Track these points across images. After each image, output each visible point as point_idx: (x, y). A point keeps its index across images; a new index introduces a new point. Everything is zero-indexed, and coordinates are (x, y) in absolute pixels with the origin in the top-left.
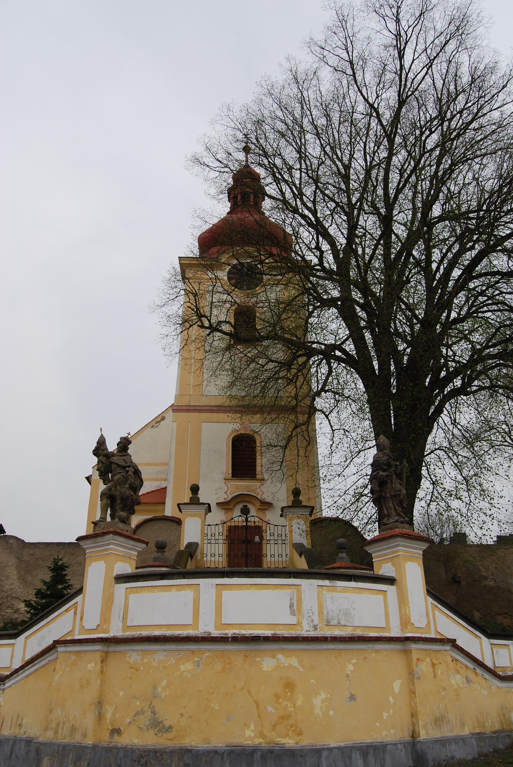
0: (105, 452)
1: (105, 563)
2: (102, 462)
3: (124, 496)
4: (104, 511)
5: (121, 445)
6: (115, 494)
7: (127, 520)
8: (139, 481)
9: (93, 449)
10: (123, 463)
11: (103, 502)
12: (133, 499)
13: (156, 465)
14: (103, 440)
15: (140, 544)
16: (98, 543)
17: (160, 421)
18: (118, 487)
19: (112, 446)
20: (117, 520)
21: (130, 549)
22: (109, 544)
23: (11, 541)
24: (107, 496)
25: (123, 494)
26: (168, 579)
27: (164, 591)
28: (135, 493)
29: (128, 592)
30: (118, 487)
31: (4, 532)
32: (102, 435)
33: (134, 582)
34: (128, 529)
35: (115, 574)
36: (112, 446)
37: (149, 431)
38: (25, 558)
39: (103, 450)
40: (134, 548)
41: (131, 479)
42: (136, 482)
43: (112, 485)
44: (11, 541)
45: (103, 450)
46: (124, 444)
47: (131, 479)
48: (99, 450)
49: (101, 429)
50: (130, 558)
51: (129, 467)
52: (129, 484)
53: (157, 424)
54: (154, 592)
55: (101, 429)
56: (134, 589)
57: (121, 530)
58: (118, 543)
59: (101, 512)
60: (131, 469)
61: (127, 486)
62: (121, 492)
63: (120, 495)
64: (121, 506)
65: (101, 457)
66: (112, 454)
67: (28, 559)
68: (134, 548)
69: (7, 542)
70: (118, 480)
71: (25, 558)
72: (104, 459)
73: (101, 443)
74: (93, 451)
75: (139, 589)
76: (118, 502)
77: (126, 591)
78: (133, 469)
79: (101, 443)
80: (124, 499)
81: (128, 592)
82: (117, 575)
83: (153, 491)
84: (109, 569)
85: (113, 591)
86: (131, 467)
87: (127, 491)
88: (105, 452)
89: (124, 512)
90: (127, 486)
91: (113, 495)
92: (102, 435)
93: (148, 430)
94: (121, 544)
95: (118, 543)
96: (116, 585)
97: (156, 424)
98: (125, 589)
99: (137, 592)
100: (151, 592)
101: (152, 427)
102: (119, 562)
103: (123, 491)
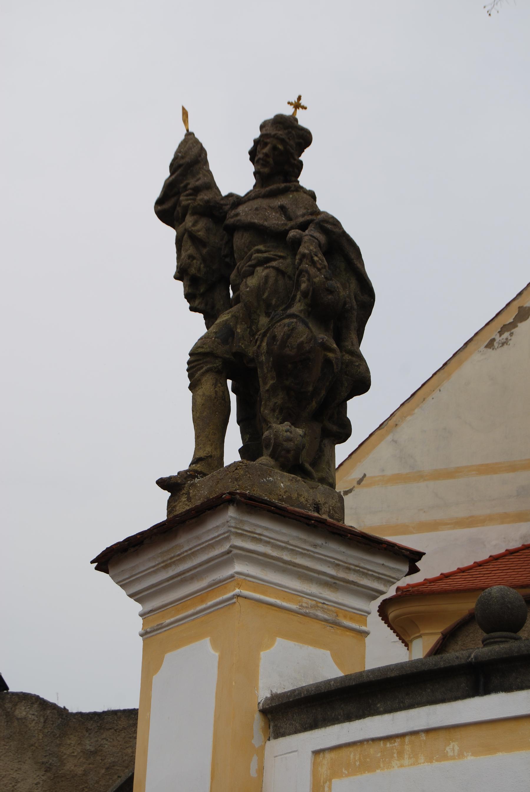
0: (204, 196)
1: (215, 644)
2: (194, 238)
3: (287, 351)
4: (209, 424)
5: (266, 150)
6: (251, 351)
7: (315, 463)
8: (353, 285)
9: (157, 192)
10: (275, 221)
11: (200, 392)
12: (328, 362)
13: (513, 468)
14: (195, 151)
15: (380, 560)
16: (183, 559)
17: (513, 325)
18: (264, 321)
19: (233, 175)
20: (265, 459)
21: (334, 584)
22: (228, 558)
23: (21, 711)
24: (218, 363)
25: (284, 343)
26: (508, 689)
27: (490, 749)
28: (339, 338)
29: (324, 770)
30: (264, 321)
31: (7, 688)
32: (189, 135)
33: (349, 718)
34: (320, 499)
35: (263, 693)
36: (233, 175)
37: (479, 361)
38: (69, 766)
39: (197, 190)
40: (352, 577)
41: (312, 271)
42: (335, 283)
43: (235, 317)
44: (21, 711)
45: (197, 190)
46: (281, 146)
47: (312, 271)
48: (178, 194)
49: (185, 114)
50: (336, 624)
51: (303, 227)
52: (305, 295)
53: (506, 335)
54: (445, 757)
55: (185, 114)
56: (353, 754)
57: (282, 500)
58: (268, 550)
59: (197, 437)
60: (310, 242)
61: (297, 308)
62: (274, 338)
63: (269, 352)
64: (279, 399)
65: (189, 221)
66: (235, 201)
67: (79, 771)
68: (352, 577)
69: (9, 717)
70: (259, 291)
71: (69, 766)
72: (200, 226)
73: (190, 163)
74: (159, 202)
75: (373, 750)
76: (267, 382)
77: (315, 765)
78: (322, 238)
79: (190, 163)
80: (290, 365)
81: (324, 770)
82: (274, 697)
83: (510, 553)
84: (238, 668)
85: (261, 770)
86: (311, 227)
87: (301, 327)
88: (204, 196)
89: (295, 424)
90: (297, 308)
91: (240, 355)
92: (189, 135)
93: (476, 357)
94: (286, 557)
95: (268, 550)
96: (274, 743)
97: (501, 333)
98: (309, 756)
99: (366, 766)
100: (430, 760)
101: (490, 344)
102: (280, 641)
103: (280, 331)
